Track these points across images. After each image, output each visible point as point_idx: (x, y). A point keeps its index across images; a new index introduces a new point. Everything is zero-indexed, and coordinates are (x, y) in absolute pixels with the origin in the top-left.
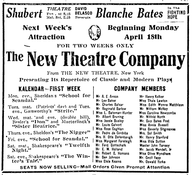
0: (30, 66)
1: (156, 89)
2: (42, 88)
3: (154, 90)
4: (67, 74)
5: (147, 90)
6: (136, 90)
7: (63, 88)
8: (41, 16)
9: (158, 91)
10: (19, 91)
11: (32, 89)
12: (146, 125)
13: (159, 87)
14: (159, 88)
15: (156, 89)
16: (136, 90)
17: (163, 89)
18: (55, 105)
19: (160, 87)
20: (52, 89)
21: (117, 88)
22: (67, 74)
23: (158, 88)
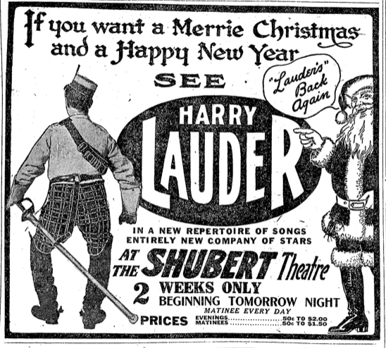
6: (336, 306)
16: (336, 306)
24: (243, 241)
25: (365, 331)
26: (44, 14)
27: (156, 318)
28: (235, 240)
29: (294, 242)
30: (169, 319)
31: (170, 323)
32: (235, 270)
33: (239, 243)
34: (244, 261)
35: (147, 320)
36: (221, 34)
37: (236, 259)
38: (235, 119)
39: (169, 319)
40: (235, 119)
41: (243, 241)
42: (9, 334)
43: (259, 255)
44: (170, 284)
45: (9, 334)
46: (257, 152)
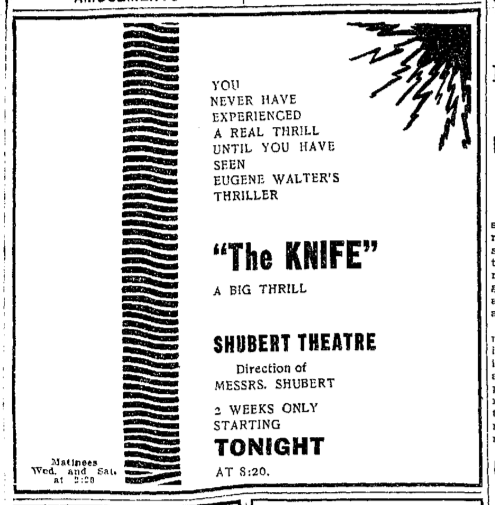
0: (216, 441)
1: (257, 343)
2: (252, 340)
3: (250, 350)
4: (286, 133)
5: (265, 346)
6: (286, 349)
7: (321, 442)
8: (218, 444)
9: (263, 353)
10: (289, 266)
11: (310, 253)
12: (218, 351)
13: (269, 338)
14: (268, 340)
15: (257, 343)
16: (286, 349)
17: (223, 343)
18: (218, 292)
19: (272, 336)
20: (340, 254)
22: (286, 133)
23: (264, 340)
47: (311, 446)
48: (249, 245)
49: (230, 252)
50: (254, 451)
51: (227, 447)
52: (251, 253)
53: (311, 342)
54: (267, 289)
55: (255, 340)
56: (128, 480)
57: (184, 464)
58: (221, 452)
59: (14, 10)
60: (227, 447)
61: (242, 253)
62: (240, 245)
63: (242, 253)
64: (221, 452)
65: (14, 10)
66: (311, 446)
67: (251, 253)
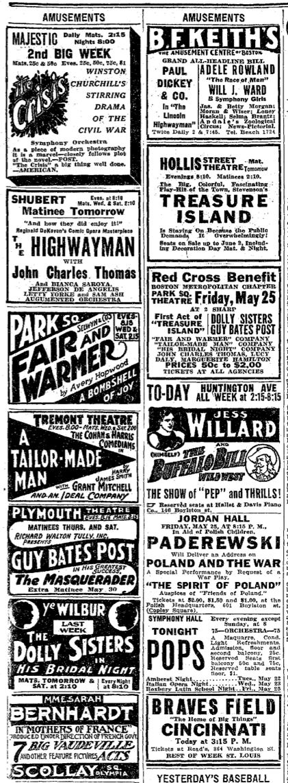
6: (186, 399)
16: (186, 399)
20: (232, 706)
21: (54, 242)
24: (177, 563)
25: (154, 300)
26: (200, 292)
27: (50, 255)
28: (156, 540)
29: (266, 565)
30: (171, 726)
31: (171, 733)
32: (98, 361)
33: (165, 548)
34: (103, 349)
35: (155, 543)
36: (184, 666)
37: (94, 353)
38: (92, 224)
39: (171, 726)
40: (92, 224)
41: (177, 563)
42: (8, 302)
43: (112, 340)
44: (175, 778)
45: (8, 302)
46: (49, 656)
47: (193, 631)
48: (104, 267)
49: (153, 584)
50: (228, 220)
51: (158, 631)
52: (104, 271)
53: (251, 493)
54: (113, 119)
55: (159, 703)
56: (133, 255)
57: (153, 464)
58: (155, 633)
59: (98, 277)
60: (158, 631)
61: (101, 271)
62: (100, 267)
63: (101, 271)
64: (155, 633)
65: (98, 277)
66: (193, 631)
67: (104, 271)
